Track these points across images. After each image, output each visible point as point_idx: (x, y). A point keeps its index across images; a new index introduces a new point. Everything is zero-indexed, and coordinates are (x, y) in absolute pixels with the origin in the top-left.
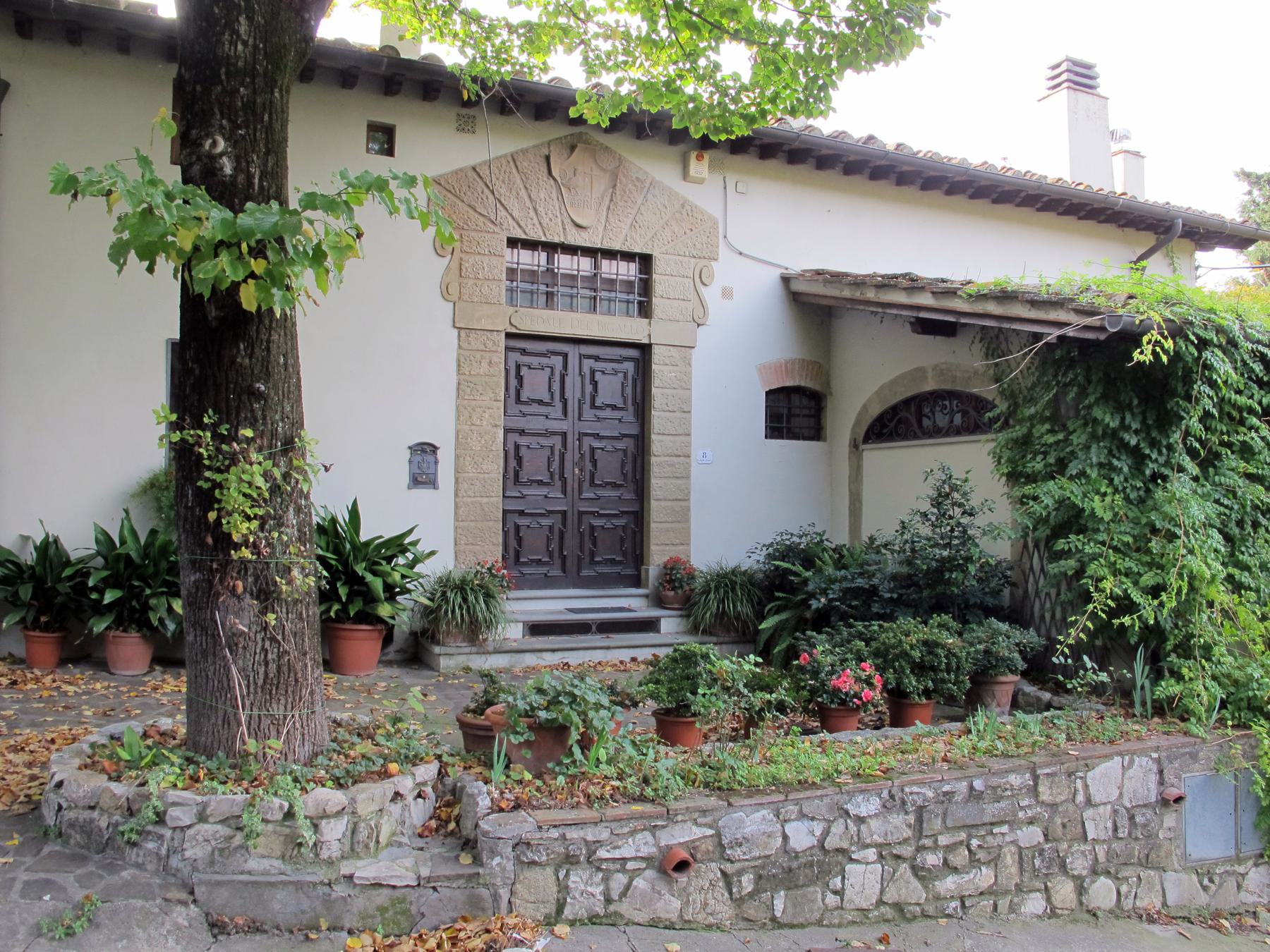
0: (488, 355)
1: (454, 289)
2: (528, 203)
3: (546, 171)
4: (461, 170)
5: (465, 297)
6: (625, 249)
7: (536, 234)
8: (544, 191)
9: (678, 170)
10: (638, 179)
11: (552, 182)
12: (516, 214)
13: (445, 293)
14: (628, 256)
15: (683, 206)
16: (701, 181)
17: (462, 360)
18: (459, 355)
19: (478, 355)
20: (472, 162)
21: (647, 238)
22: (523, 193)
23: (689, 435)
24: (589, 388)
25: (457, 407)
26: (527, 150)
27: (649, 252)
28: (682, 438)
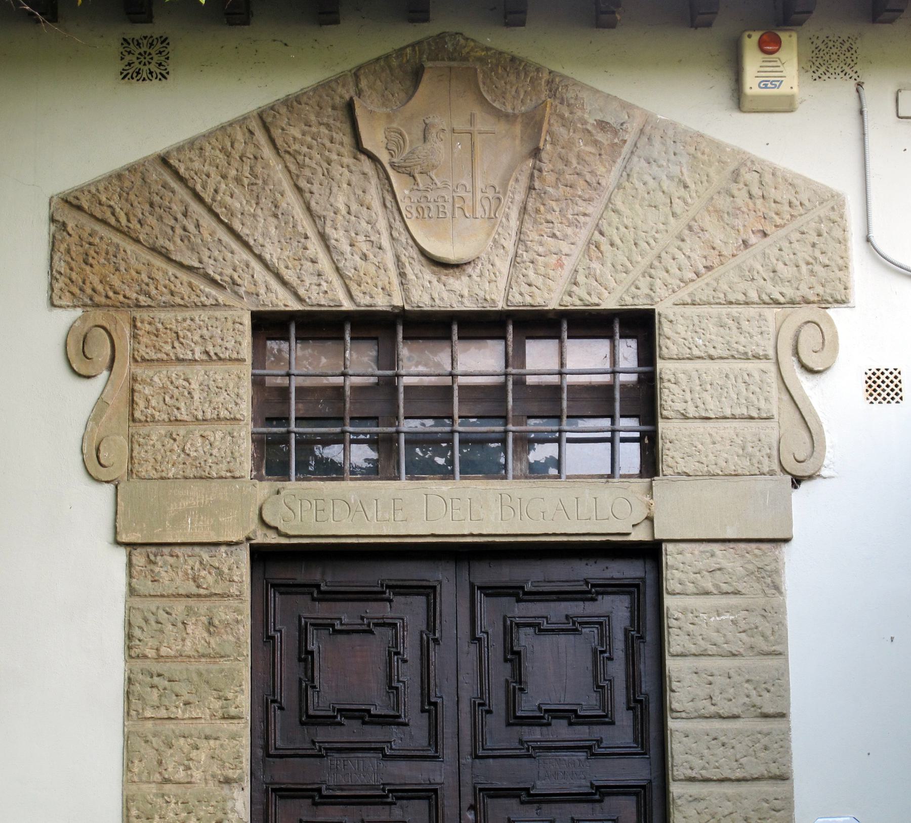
0: (202, 607)
1: (115, 454)
2: (305, 225)
3: (347, 140)
4: (132, 169)
5: (145, 469)
6: (574, 303)
7: (327, 294)
8: (347, 193)
9: (721, 85)
10: (603, 125)
11: (367, 165)
12: (271, 252)
13: (94, 465)
14: (590, 323)
15: (736, 176)
16: (787, 105)
17: (138, 620)
18: (129, 610)
19: (179, 608)
20: (160, 146)
21: (636, 272)
22: (291, 202)
23: (783, 778)
24: (500, 672)
25: (127, 737)
26: (298, 99)
27: (642, 304)
28: (766, 788)
